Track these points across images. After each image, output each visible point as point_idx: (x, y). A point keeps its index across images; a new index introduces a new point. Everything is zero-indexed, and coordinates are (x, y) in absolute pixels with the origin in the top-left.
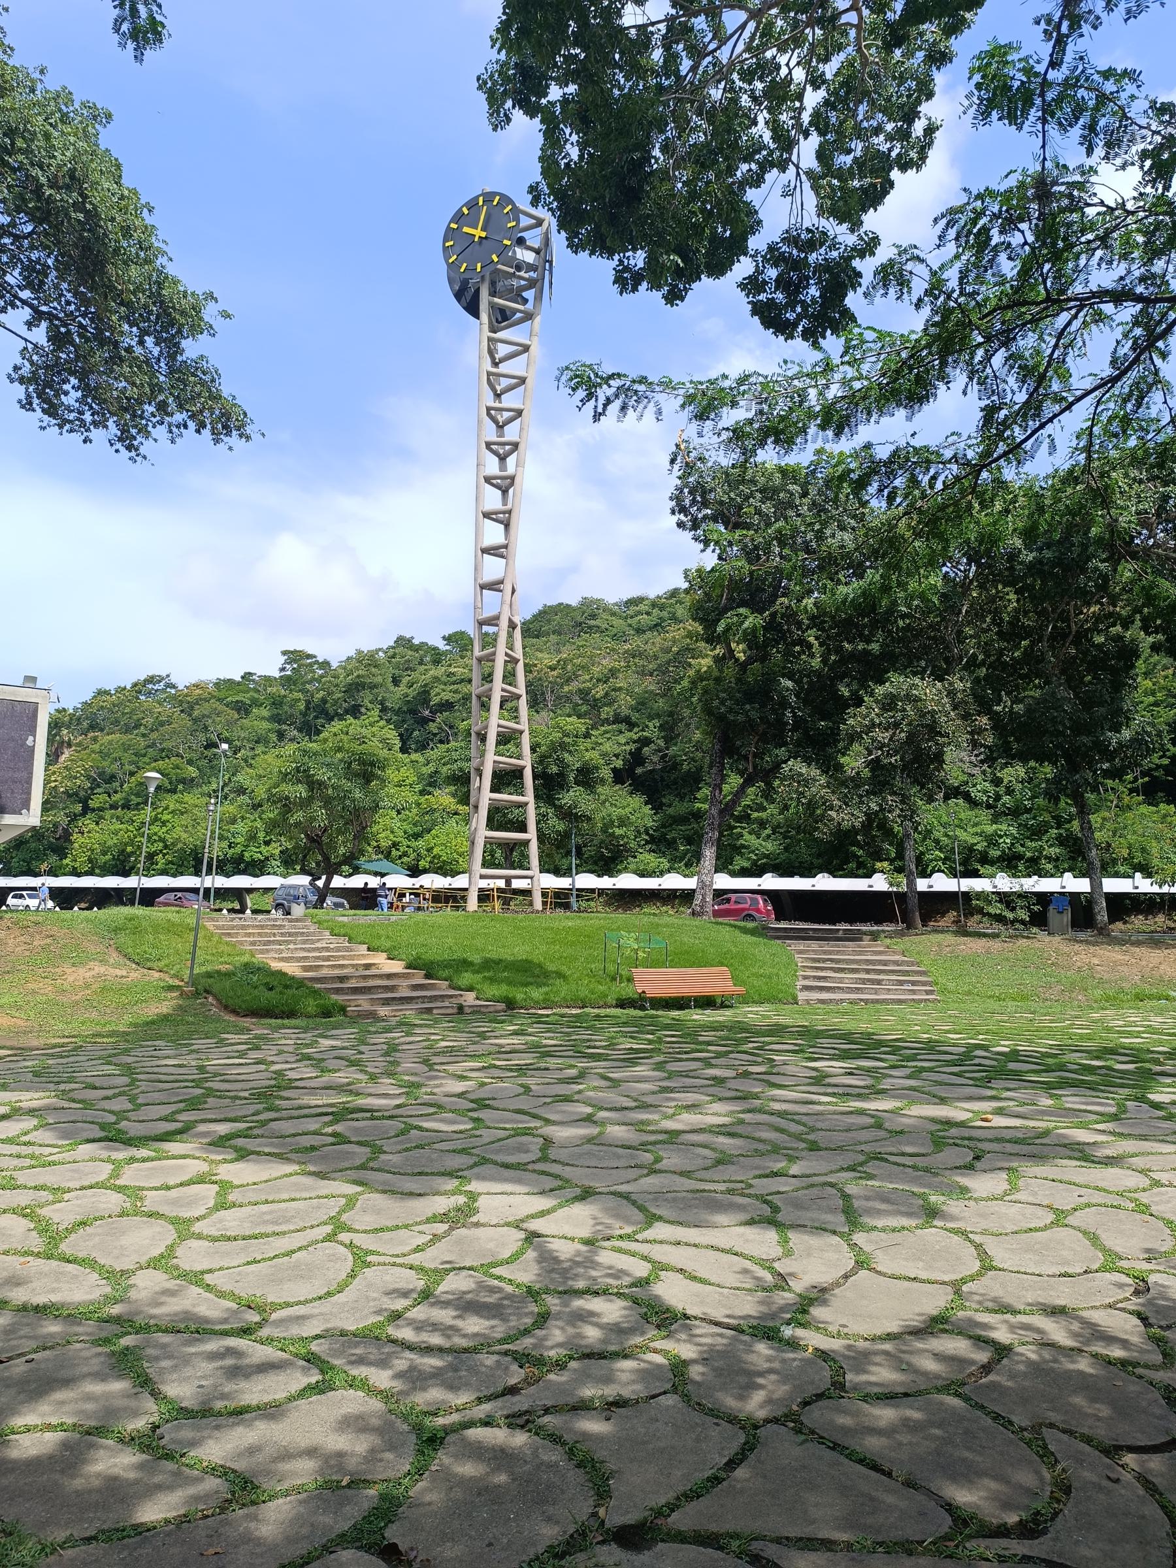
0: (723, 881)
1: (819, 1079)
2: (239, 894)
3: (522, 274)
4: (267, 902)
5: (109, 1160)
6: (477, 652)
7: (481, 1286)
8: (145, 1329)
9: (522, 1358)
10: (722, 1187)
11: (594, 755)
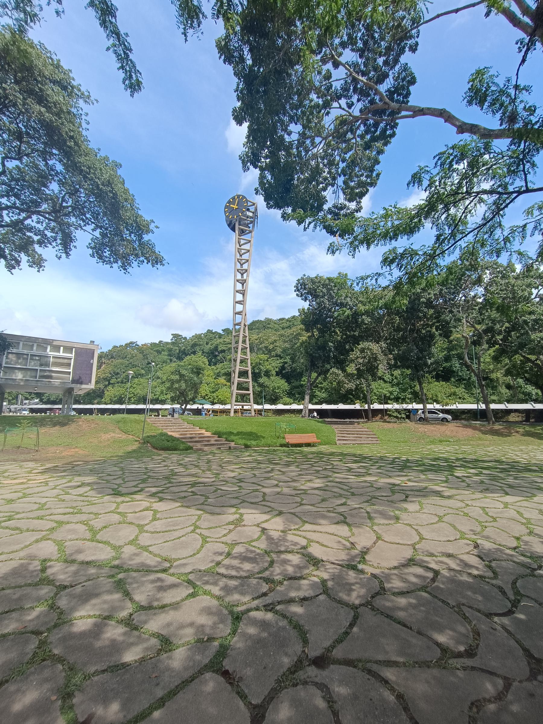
0: (311, 407)
1: (350, 470)
2: (157, 410)
4: (166, 413)
5: (115, 502)
6: (234, 334)
7: (247, 550)
8: (127, 570)
9: (267, 580)
10: (325, 510)
11: (270, 366)
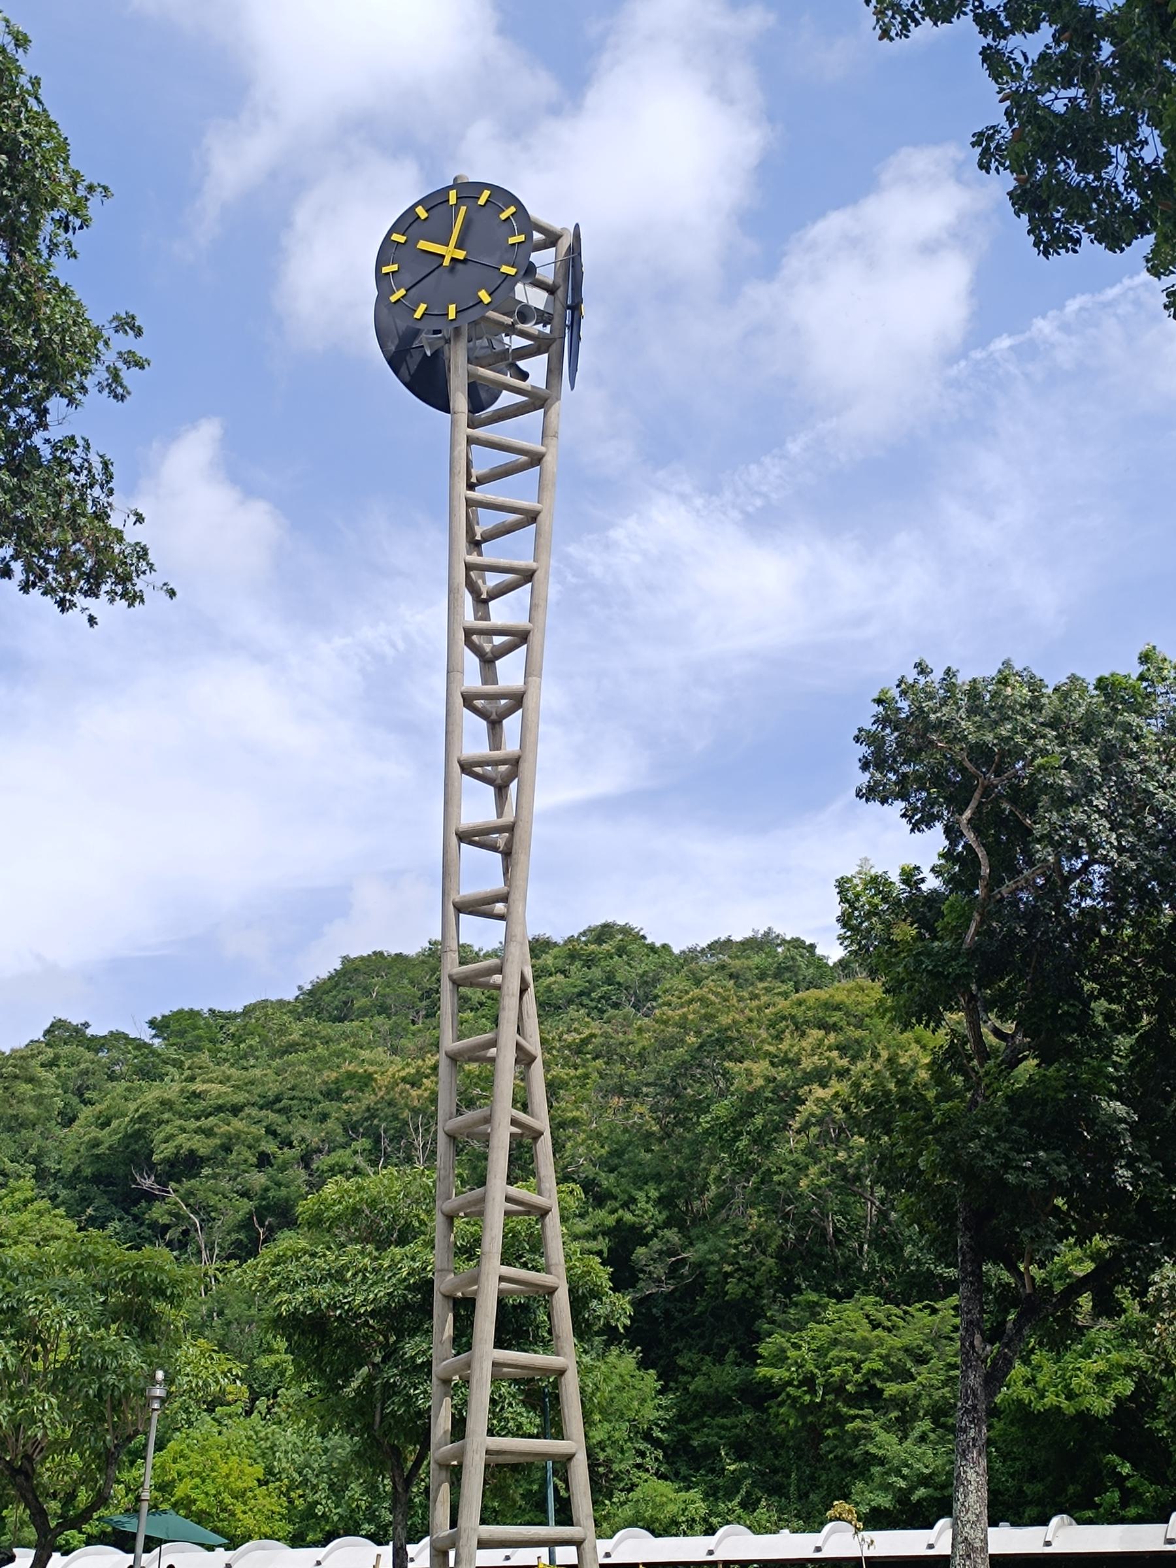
3: (527, 327)
